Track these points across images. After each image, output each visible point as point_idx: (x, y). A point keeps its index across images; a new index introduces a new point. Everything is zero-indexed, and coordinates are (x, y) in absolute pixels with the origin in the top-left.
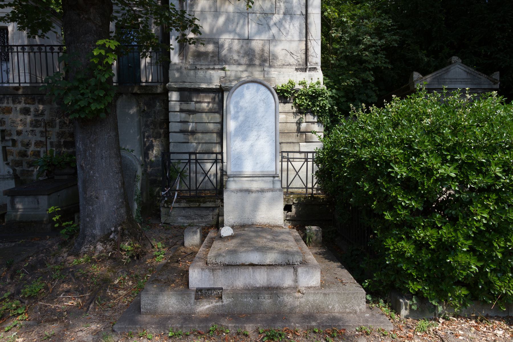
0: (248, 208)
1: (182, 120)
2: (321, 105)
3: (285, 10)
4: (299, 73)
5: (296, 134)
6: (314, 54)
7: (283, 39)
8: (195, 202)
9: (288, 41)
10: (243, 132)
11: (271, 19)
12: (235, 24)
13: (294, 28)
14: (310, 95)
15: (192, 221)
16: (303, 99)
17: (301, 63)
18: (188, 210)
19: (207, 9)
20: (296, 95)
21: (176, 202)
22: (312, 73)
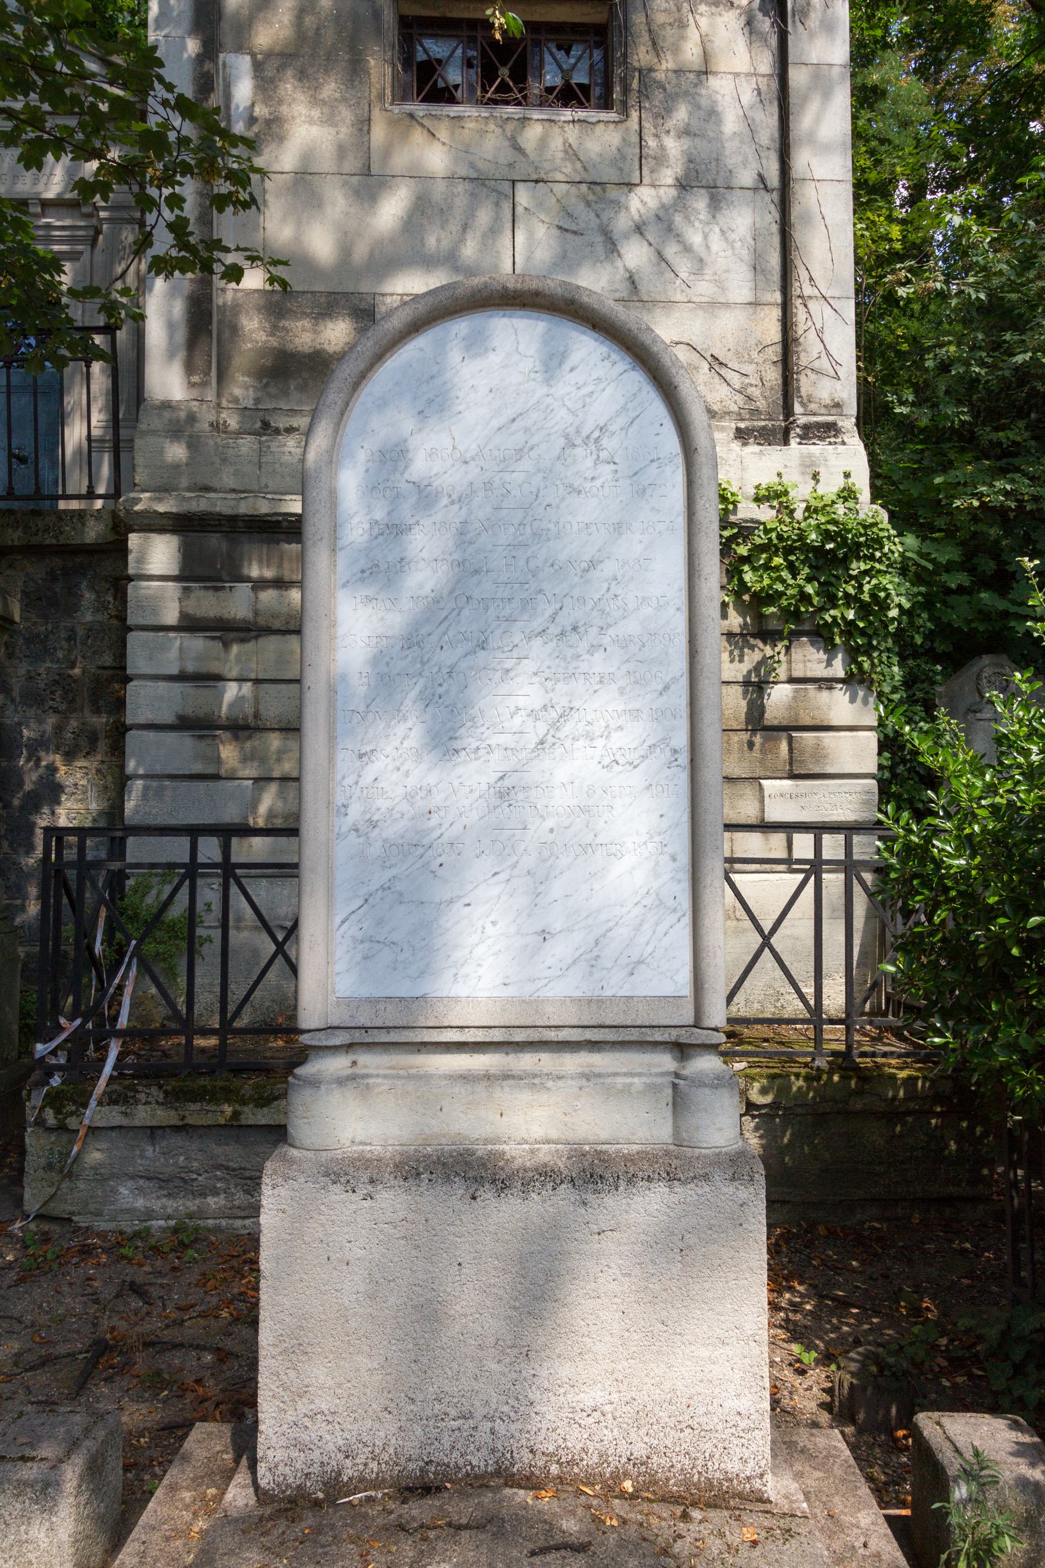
0: (474, 1302)
1: (191, 668)
2: (866, 597)
3: (687, 175)
4: (753, 448)
5: (745, 736)
6: (824, 364)
7: (679, 297)
8: (213, 1096)
9: (700, 305)
10: (434, 684)
11: (617, 205)
12: (454, 227)
13: (727, 242)
14: (814, 549)
15: (192, 1205)
16: (777, 569)
17: (761, 404)
18: (177, 1141)
19: (326, 162)
20: (743, 550)
21: (111, 1099)
22: (817, 449)
